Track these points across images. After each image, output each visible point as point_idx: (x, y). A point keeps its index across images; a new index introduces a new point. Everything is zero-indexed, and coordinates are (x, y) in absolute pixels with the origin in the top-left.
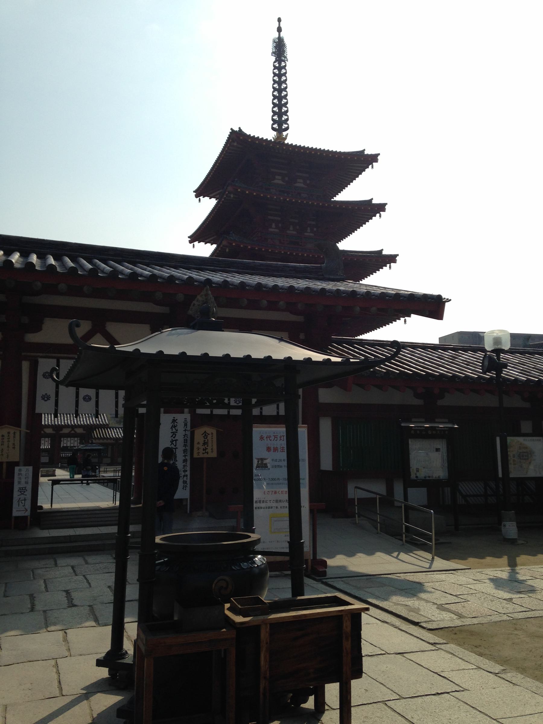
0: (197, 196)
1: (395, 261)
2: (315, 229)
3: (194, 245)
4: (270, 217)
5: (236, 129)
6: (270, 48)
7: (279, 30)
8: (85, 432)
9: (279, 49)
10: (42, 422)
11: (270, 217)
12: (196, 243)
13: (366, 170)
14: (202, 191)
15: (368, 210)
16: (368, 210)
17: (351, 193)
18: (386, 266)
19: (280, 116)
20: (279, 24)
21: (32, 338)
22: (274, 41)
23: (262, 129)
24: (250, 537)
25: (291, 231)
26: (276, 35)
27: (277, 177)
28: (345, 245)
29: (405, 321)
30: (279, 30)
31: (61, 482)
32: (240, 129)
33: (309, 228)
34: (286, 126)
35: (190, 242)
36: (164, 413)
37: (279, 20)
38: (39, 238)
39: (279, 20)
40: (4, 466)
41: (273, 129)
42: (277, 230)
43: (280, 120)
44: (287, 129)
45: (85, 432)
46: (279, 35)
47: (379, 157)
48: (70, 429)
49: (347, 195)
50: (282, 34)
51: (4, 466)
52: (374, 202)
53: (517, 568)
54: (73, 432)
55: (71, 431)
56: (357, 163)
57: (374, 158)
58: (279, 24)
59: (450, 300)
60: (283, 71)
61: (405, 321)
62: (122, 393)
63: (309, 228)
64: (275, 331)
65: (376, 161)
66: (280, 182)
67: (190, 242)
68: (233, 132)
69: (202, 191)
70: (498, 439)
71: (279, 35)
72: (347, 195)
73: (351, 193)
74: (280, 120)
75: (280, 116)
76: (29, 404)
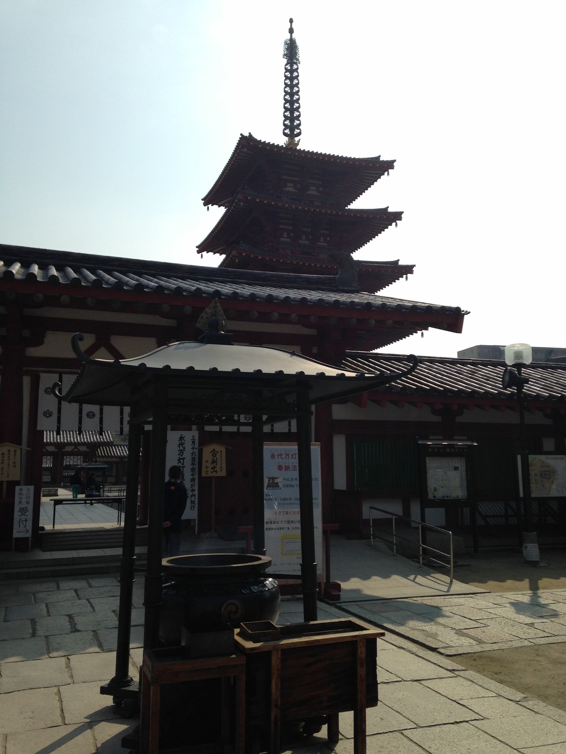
0: (205, 204)
1: (411, 272)
2: (328, 239)
3: (202, 255)
4: (281, 226)
5: (246, 134)
6: (281, 49)
7: (291, 31)
8: (88, 450)
9: (291, 51)
10: (43, 439)
11: (281, 226)
12: (204, 253)
13: (382, 177)
14: (211, 199)
15: (383, 219)
16: (383, 219)
17: (366, 201)
18: (402, 277)
19: (292, 121)
20: (291, 25)
21: (34, 352)
22: (286, 43)
23: (273, 134)
24: (260, 559)
25: (304, 241)
26: (288, 36)
27: (289, 184)
28: (359, 255)
29: (422, 335)
30: (291, 31)
31: (64, 502)
32: (250, 135)
33: (322, 238)
34: (298, 131)
35: (199, 252)
36: (171, 430)
37: (291, 21)
38: (41, 248)
39: (291, 21)
40: (5, 485)
41: (285, 134)
42: (288, 240)
43: (292, 125)
44: (299, 134)
45: (88, 450)
46: (291, 36)
47: (395, 164)
48: (73, 447)
49: (362, 203)
50: (294, 36)
51: (5, 485)
52: (389, 210)
53: (538, 592)
54: (76, 450)
55: (74, 449)
56: (372, 170)
57: (390, 165)
58: (291, 25)
59: (469, 312)
60: (295, 74)
61: (422, 335)
62: (127, 410)
63: (322, 238)
64: (287, 344)
65: (392, 168)
66: (292, 190)
67: (199, 252)
68: (243, 137)
69: (211, 199)
70: (519, 457)
71: (291, 36)
72: (362, 203)
73: (366, 201)
74: (292, 125)
75: (292, 121)
76: (30, 420)
